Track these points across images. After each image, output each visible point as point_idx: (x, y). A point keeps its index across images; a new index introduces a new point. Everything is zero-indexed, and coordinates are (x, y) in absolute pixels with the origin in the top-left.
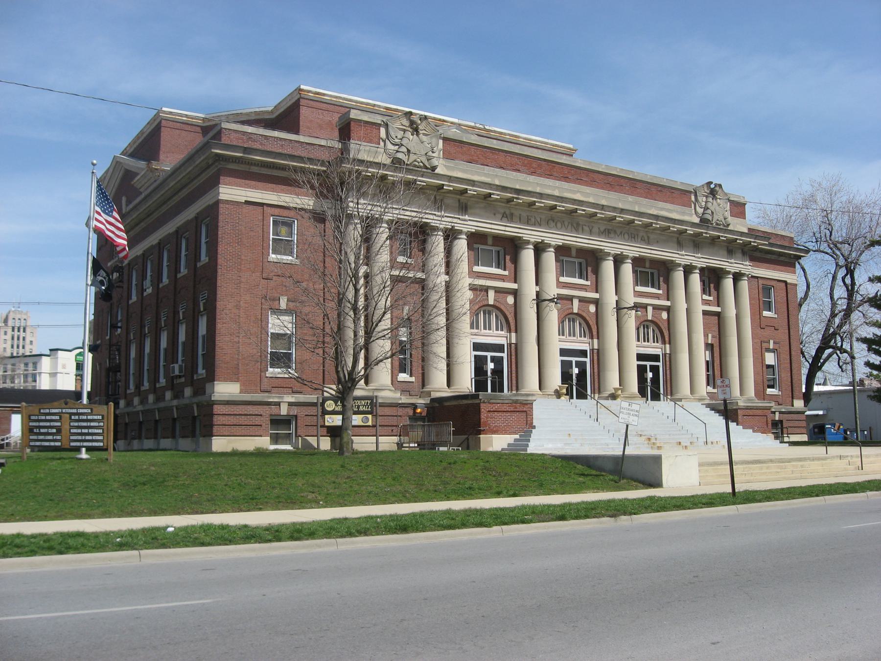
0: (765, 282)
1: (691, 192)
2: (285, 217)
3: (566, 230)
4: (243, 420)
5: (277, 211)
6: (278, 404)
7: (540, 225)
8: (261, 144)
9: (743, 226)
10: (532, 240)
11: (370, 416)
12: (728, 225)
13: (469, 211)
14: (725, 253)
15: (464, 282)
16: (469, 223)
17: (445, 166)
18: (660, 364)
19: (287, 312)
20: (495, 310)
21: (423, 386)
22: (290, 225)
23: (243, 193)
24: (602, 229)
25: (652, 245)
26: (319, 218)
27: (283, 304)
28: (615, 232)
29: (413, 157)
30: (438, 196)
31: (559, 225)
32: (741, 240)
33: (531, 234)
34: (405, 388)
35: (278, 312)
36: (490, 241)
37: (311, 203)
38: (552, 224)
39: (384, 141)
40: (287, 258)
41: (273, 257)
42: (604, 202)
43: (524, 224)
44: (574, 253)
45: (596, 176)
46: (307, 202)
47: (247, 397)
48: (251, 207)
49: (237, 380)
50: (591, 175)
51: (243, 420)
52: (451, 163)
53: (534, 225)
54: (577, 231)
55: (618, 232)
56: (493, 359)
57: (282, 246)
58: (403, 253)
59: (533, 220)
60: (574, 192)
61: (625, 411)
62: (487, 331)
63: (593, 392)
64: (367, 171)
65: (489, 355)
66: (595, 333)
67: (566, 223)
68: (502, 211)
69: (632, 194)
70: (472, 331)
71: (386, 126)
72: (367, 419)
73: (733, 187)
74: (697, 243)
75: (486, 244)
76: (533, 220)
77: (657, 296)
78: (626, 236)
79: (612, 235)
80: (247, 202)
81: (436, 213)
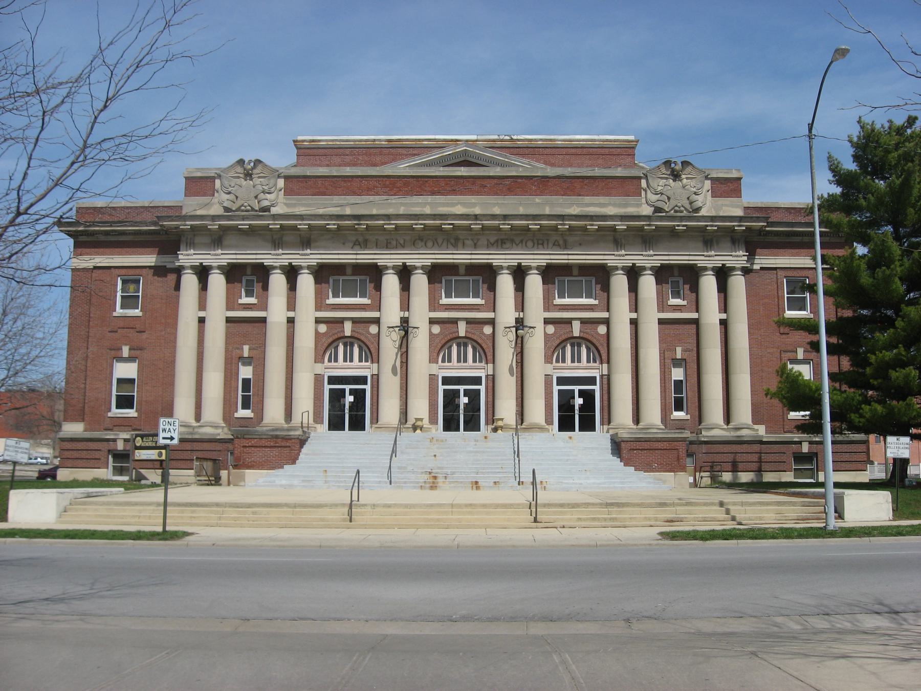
0: (790, 273)
1: (640, 178)
2: (131, 276)
3: (440, 247)
4: (84, 454)
5: (123, 272)
6: (115, 440)
7: (403, 247)
8: (110, 215)
9: (737, 207)
10: (391, 264)
11: (164, 451)
12: (697, 210)
13: (312, 245)
14: (700, 244)
15: (536, 313)
16: (195, 257)
17: (285, 204)
18: (597, 388)
19: (131, 359)
20: (583, 342)
21: (700, 422)
22: (137, 282)
23: (787, 261)
24: (492, 240)
25: (571, 249)
26: (159, 271)
27: (800, 354)
28: (512, 241)
29: (673, 202)
30: (279, 237)
31: (430, 244)
32: (741, 227)
33: (268, 257)
34: (680, 425)
35: (121, 359)
36: (575, 272)
37: (154, 260)
38: (421, 244)
39: (645, 191)
40: (137, 312)
41: (119, 311)
42: (477, 211)
43: (382, 248)
44: (462, 270)
45: (485, 182)
46: (149, 259)
47: (88, 435)
48: (100, 271)
49: (83, 420)
50: (479, 182)
51: (84, 454)
52: (294, 199)
53: (396, 248)
54: (455, 246)
55: (517, 240)
56: (582, 393)
57: (129, 302)
58: (676, 294)
59: (394, 243)
60: (453, 205)
61: (11, 449)
62: (348, 363)
63: (602, 424)
64: (564, 225)
65: (576, 388)
66: (604, 357)
67: (440, 241)
68: (354, 239)
69: (542, 194)
70: (459, 364)
71: (646, 177)
72: (161, 453)
73: (218, 160)
74: (645, 237)
75: (345, 274)
76: (394, 243)
77: (590, 308)
78: (530, 244)
79: (508, 245)
80: (95, 268)
81: (705, 253)
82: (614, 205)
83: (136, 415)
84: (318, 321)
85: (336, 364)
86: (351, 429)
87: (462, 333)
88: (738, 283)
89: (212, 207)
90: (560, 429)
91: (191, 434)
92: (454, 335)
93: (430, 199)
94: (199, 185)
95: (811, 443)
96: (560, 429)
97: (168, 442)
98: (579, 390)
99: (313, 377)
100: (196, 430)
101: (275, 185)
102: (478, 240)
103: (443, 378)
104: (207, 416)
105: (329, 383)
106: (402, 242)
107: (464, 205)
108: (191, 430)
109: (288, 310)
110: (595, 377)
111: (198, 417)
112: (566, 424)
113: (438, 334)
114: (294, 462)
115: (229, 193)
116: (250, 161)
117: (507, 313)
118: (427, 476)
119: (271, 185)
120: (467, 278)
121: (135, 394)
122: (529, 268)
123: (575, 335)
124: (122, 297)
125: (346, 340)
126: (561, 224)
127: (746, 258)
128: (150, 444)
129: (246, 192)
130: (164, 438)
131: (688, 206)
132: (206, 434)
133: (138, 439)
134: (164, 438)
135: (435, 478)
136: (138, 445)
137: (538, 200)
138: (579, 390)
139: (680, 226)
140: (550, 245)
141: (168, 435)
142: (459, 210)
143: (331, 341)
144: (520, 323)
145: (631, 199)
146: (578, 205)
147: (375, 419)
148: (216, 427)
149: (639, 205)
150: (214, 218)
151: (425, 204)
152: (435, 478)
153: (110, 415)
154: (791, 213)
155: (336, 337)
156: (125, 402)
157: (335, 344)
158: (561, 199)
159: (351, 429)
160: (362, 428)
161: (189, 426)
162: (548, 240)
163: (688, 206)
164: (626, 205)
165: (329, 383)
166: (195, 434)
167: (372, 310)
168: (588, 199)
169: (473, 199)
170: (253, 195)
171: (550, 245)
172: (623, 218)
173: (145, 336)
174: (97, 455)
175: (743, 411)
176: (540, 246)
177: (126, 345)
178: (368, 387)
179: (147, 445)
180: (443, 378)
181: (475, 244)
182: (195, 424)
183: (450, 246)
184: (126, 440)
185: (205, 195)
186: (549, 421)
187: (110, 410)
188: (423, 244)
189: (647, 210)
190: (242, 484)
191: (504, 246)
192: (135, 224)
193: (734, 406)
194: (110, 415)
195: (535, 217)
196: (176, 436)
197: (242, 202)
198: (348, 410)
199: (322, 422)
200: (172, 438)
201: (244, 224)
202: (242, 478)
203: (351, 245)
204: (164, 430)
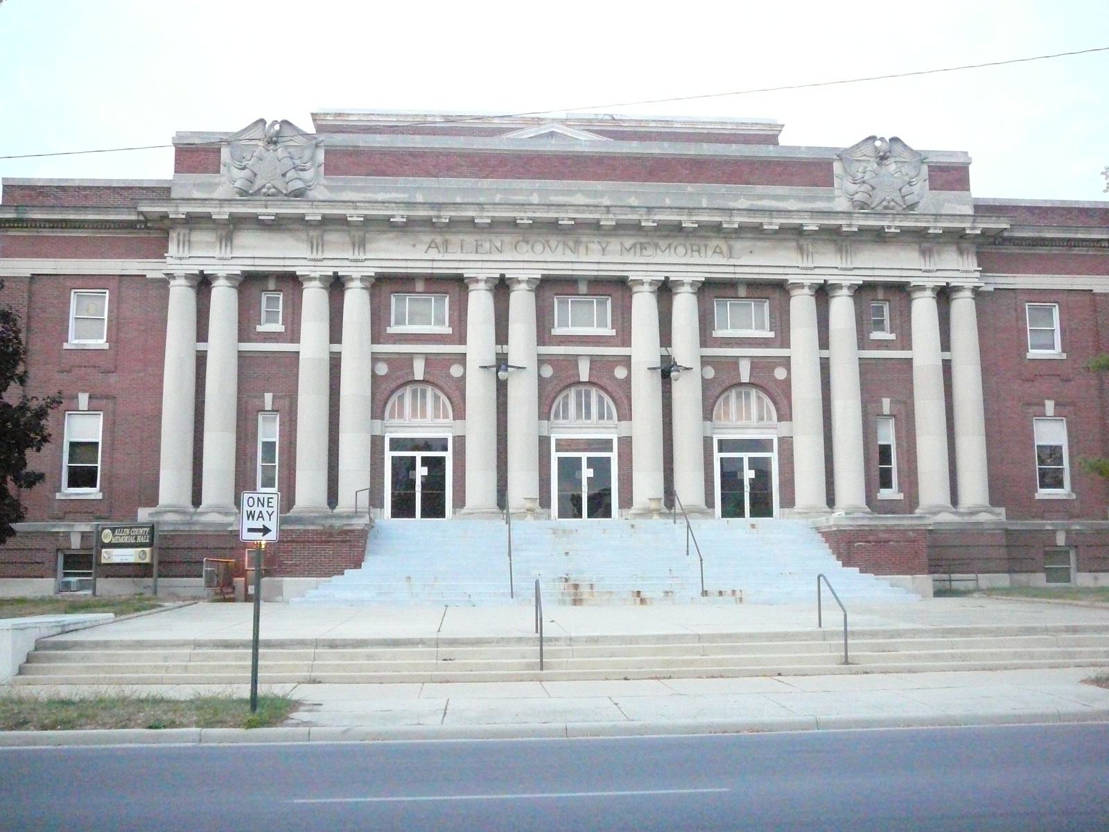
11: (147, 550)
17: (326, 187)
33: (478, 262)
52: (340, 180)
56: (753, 463)
60: (571, 193)
67: (553, 246)
82: (798, 198)
83: (100, 496)
84: (375, 358)
85: (588, 421)
86: (753, 514)
87: (584, 377)
88: (963, 307)
89: (218, 191)
90: (394, 515)
91: (189, 524)
92: (572, 380)
93: (538, 183)
94: (195, 155)
95: (113, 530)
96: (394, 515)
97: (258, 536)
98: (589, 459)
99: (369, 438)
100: (195, 518)
101: (312, 158)
102: (608, 243)
103: (392, 440)
104: (208, 497)
105: (392, 449)
106: (498, 244)
107: (588, 193)
108: (188, 518)
109: (331, 342)
110: (446, 440)
111: (197, 500)
112: (732, 508)
113: (616, 379)
114: (357, 565)
115: (244, 168)
116: (275, 122)
117: (644, 349)
118: (563, 585)
119: (305, 159)
120: (589, 298)
121: (99, 465)
122: (680, 283)
123: (582, 380)
124: (411, 322)
125: (414, 386)
126: (728, 222)
127: (978, 274)
128: (125, 540)
129: (269, 167)
130: (250, 530)
131: (899, 200)
132: (211, 524)
133: (107, 531)
134: (250, 530)
135: (576, 586)
136: (106, 541)
137: (690, 188)
138: (589, 459)
139: (891, 225)
140: (710, 252)
141: (258, 524)
142: (580, 199)
143: (720, 385)
144: (502, 362)
145: (820, 191)
146: (747, 197)
147: (460, 501)
148: (226, 514)
149: (830, 199)
150: (222, 202)
151: (531, 192)
152: (576, 586)
153: (58, 496)
154: (1033, 214)
155: (402, 381)
156: (82, 477)
157: (399, 393)
158: (722, 188)
159: (425, 514)
160: (769, 513)
161: (184, 513)
162: (706, 246)
163: (899, 200)
164: (813, 199)
165: (392, 449)
166: (194, 524)
167: (285, 341)
168: (760, 189)
169: (599, 185)
170: (279, 172)
171: (710, 252)
172: (814, 213)
173: (113, 378)
174: (39, 557)
175: (974, 489)
176: (696, 254)
177: (84, 391)
178: (448, 456)
179: (121, 541)
180: (392, 440)
181: (604, 250)
182: (192, 509)
183: (568, 251)
184: (84, 535)
185: (205, 170)
186: (710, 503)
187: (59, 489)
188: (529, 247)
189: (841, 204)
190: (279, 598)
191: (645, 252)
192: (864, 213)
193: (953, 479)
194: (58, 496)
195: (691, 210)
196: (273, 525)
197: (264, 182)
198: (420, 488)
199: (382, 506)
200: (265, 530)
201: (267, 212)
202: (279, 591)
203: (425, 247)
204: (251, 515)
